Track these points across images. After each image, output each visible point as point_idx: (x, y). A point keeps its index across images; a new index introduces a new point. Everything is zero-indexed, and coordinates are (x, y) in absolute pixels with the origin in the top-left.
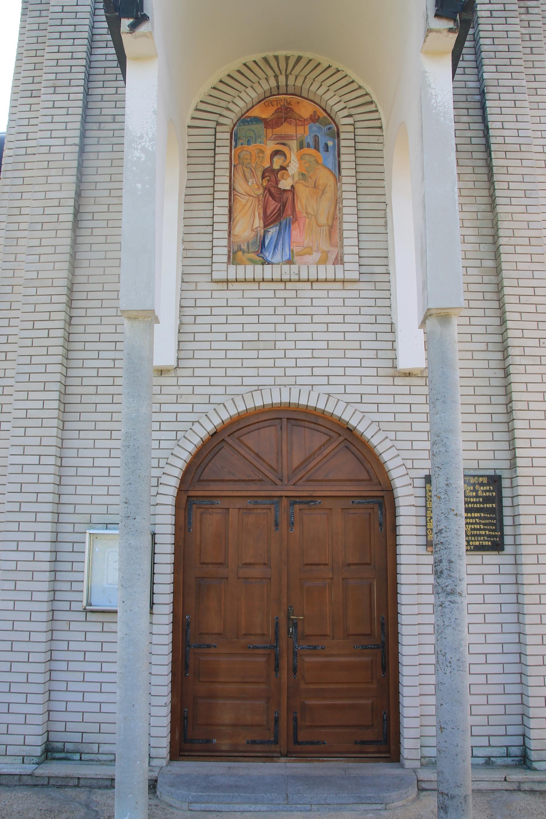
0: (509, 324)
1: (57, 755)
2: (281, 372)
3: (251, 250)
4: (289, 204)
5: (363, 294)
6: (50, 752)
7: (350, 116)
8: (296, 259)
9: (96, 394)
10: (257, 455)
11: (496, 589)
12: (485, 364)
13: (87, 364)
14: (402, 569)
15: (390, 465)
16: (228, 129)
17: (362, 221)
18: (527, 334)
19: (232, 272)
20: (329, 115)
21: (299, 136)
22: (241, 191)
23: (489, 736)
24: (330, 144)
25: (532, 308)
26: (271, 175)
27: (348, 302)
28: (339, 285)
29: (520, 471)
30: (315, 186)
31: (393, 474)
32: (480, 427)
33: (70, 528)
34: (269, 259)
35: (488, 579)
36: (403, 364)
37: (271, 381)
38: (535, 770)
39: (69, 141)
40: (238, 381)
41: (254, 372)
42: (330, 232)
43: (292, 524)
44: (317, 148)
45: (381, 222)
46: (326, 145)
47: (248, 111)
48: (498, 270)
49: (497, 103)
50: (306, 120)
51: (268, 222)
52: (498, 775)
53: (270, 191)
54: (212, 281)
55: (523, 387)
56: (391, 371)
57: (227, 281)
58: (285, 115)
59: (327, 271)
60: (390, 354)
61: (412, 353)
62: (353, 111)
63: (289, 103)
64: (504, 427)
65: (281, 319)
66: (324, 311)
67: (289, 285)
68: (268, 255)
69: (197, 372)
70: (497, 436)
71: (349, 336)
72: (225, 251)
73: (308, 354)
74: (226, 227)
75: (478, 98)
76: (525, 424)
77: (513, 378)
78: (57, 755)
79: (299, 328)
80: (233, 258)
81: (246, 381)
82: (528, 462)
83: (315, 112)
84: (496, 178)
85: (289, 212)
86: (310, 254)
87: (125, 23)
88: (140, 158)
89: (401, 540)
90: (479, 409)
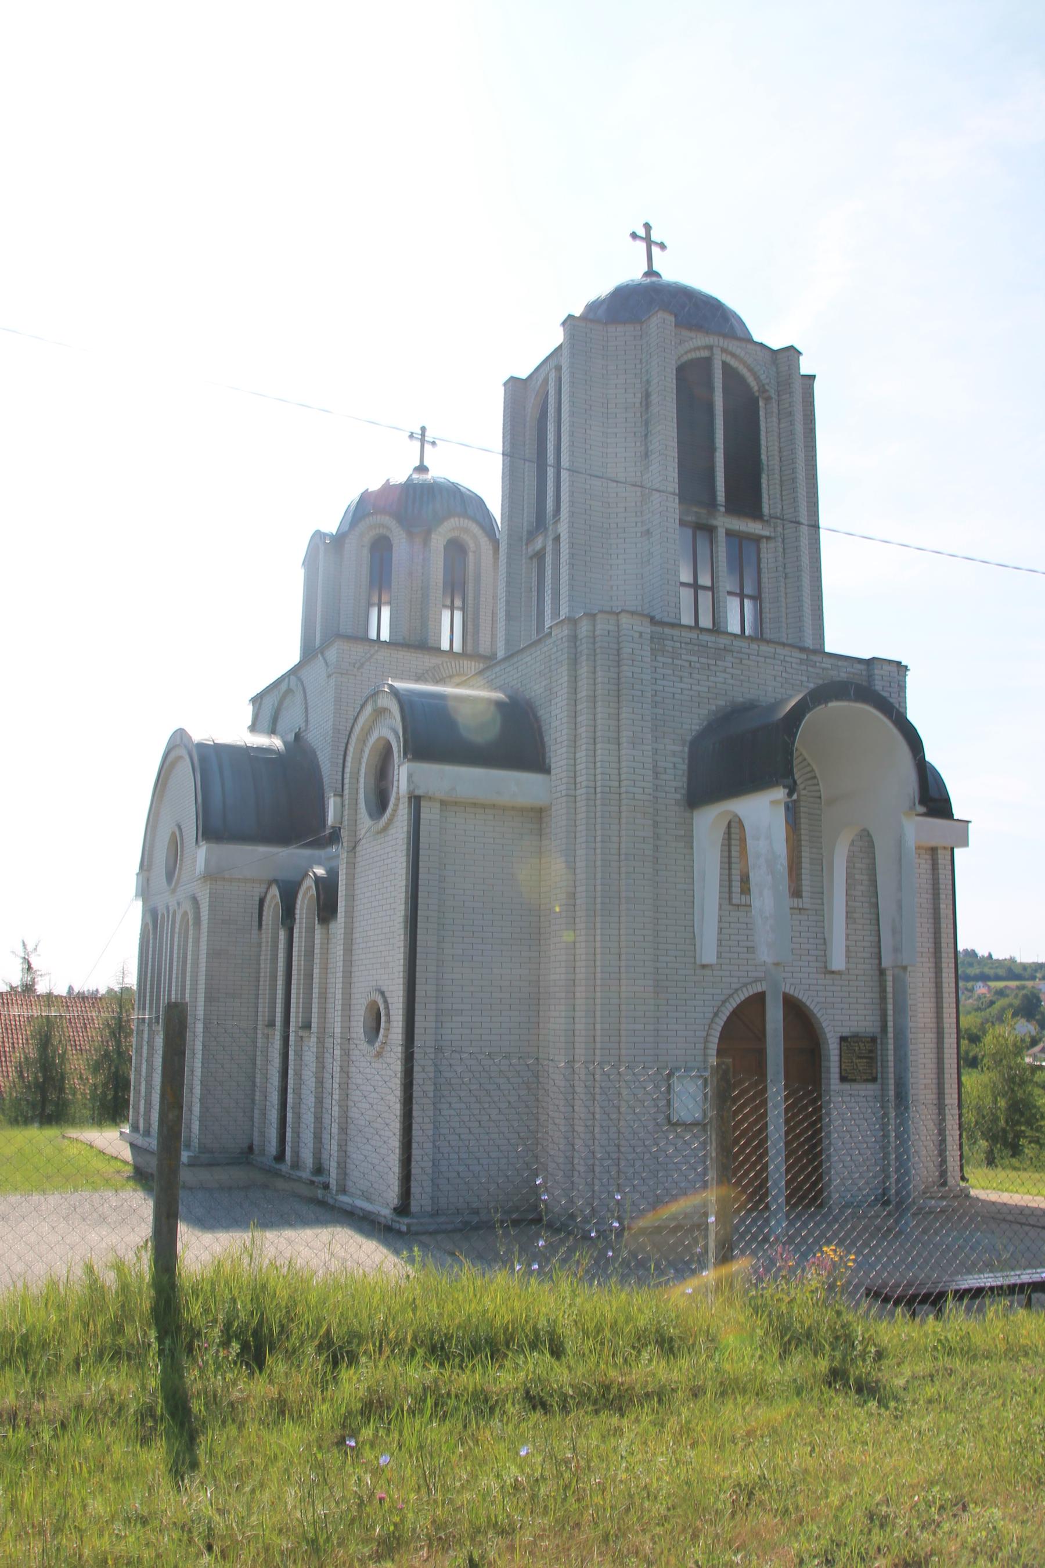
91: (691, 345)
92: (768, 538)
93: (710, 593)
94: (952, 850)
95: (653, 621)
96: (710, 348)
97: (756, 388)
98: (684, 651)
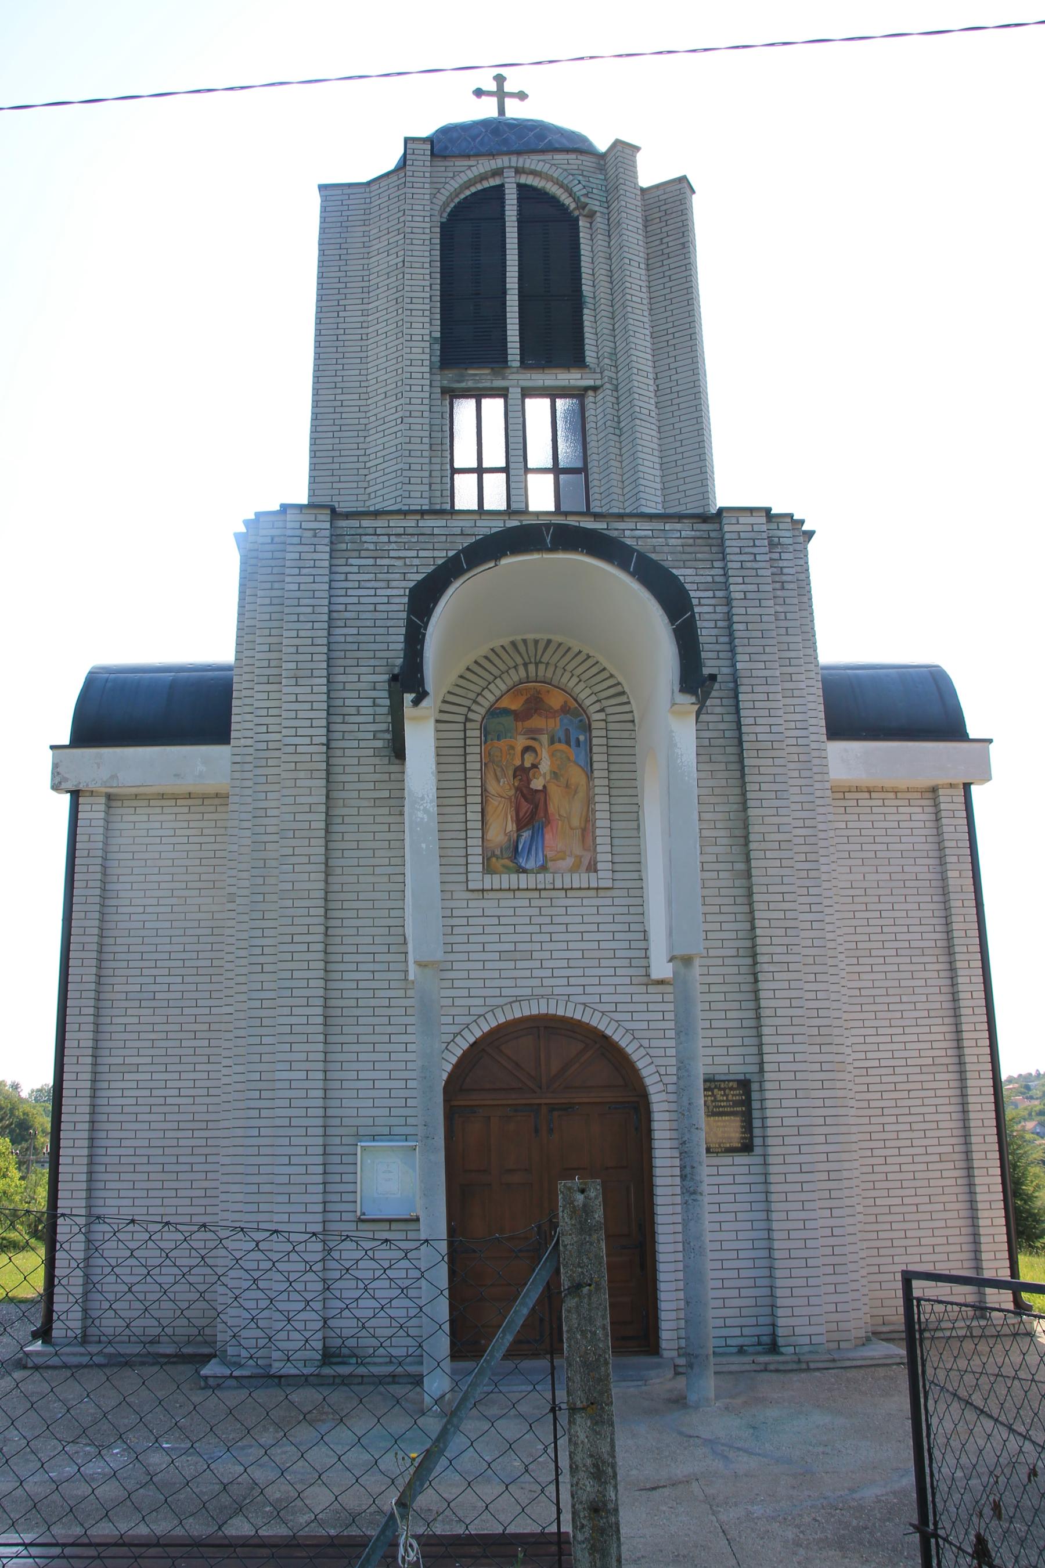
0: (758, 932)
1: (334, 1360)
2: (537, 982)
3: (505, 856)
4: (542, 805)
5: (617, 901)
6: (328, 1356)
7: (602, 710)
8: (550, 864)
9: (357, 1007)
10: (517, 1064)
11: (746, 1188)
12: (735, 970)
13: (346, 976)
14: (657, 1172)
15: (644, 1073)
16: (477, 725)
17: (615, 825)
18: (775, 941)
19: (488, 882)
20: (580, 706)
21: (550, 729)
22: (493, 792)
23: (741, 1327)
24: (582, 738)
25: (781, 915)
26: (523, 773)
27: (602, 910)
28: (593, 893)
29: (767, 1076)
30: (567, 786)
31: (648, 1081)
32: (731, 1033)
33: (337, 1140)
34: (523, 865)
35: (738, 1179)
36: (656, 975)
37: (528, 991)
38: (782, 1354)
39: (316, 740)
40: (497, 992)
41: (512, 983)
42: (583, 836)
43: (551, 1131)
44: (568, 743)
45: (634, 825)
46: (578, 739)
47: (497, 701)
48: (748, 875)
49: (750, 697)
50: (556, 711)
51: (521, 824)
52: (748, 1359)
53: (522, 792)
54: (468, 890)
55: (771, 994)
56: (644, 980)
57: (483, 890)
58: (535, 705)
59: (580, 880)
60: (644, 963)
61: (661, 968)
62: (605, 703)
63: (539, 692)
64: (754, 1032)
65: (537, 929)
66: (579, 919)
67: (544, 894)
68: (522, 861)
69: (457, 984)
70: (747, 1041)
71: (603, 945)
72: (480, 859)
73: (564, 963)
74: (479, 833)
75: (731, 685)
76: (773, 1030)
77: (761, 985)
78: (334, 1360)
79: (555, 937)
80: (488, 869)
81: (505, 992)
82: (775, 1067)
83: (565, 702)
84: (748, 779)
85: (542, 815)
86: (563, 859)
87: (408, 697)
88: (423, 819)
89: (656, 1144)
90: (730, 1015)
91: (463, 178)
92: (595, 389)
93: (504, 475)
94: (967, 787)
95: (335, 514)
96: (498, 172)
97: (573, 206)
98: (394, 546)
